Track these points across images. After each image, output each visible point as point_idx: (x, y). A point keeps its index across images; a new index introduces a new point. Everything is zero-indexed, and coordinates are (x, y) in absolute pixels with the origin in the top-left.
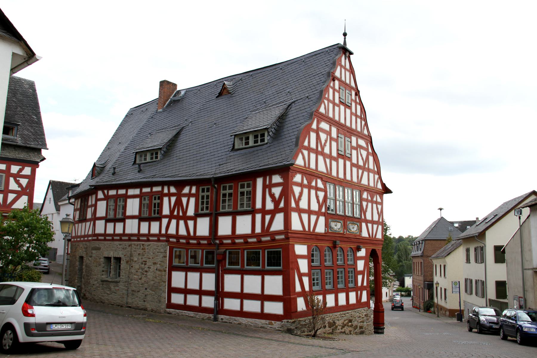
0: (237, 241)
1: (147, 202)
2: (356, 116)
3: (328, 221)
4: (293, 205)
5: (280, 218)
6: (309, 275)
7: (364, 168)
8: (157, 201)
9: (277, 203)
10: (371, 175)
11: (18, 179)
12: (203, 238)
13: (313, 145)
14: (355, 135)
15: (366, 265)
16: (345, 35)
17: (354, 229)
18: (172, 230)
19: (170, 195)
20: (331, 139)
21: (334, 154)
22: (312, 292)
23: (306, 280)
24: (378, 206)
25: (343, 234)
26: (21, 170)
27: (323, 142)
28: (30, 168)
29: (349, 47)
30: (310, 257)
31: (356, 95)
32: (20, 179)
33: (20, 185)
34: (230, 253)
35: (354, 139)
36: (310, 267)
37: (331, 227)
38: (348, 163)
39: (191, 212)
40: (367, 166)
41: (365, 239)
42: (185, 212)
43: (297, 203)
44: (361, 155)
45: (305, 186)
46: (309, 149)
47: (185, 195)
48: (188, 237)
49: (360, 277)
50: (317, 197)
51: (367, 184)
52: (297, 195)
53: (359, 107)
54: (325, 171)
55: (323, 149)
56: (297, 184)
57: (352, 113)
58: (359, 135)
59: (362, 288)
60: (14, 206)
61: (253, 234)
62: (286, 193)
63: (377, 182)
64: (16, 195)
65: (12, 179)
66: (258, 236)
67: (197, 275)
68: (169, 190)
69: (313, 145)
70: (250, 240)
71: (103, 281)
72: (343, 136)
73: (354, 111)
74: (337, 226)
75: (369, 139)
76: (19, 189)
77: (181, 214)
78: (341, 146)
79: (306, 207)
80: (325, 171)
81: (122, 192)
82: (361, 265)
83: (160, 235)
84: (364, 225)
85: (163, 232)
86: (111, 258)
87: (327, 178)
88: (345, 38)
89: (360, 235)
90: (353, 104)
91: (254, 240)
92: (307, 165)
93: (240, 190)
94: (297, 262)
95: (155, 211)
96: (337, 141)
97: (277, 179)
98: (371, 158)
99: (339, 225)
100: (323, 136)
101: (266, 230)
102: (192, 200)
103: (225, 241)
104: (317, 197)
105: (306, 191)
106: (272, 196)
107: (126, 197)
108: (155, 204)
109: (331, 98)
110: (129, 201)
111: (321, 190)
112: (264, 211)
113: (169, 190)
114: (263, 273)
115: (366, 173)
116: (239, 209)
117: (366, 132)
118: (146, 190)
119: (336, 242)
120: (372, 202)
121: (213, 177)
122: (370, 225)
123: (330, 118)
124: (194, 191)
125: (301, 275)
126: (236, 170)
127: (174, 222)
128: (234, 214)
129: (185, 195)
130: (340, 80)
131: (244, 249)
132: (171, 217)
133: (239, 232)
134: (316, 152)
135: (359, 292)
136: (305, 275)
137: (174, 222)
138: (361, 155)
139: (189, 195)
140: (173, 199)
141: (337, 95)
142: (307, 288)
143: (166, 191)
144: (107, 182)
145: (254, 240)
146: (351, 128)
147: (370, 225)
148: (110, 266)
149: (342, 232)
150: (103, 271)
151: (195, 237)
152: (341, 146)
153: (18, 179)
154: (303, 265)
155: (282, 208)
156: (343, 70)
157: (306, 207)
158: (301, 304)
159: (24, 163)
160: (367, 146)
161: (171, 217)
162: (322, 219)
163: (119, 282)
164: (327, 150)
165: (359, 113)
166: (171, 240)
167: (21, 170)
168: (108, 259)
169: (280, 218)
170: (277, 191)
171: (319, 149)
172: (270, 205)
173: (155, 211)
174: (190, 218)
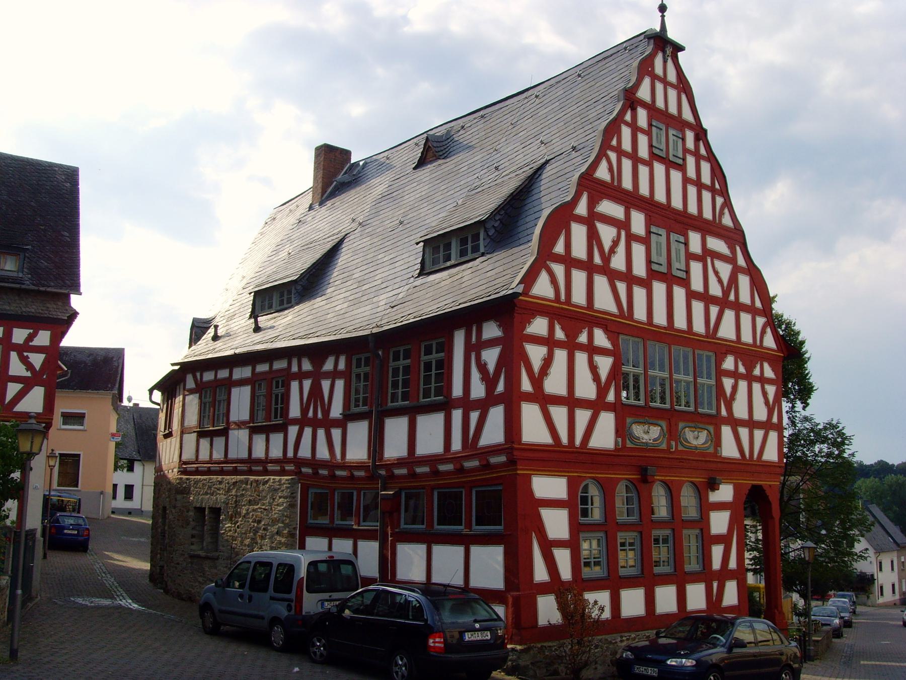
0: (419, 470)
1: (264, 391)
2: (700, 186)
3: (624, 423)
4: (526, 385)
5: (497, 414)
6: (573, 544)
7: (723, 303)
8: (281, 390)
9: (490, 382)
10: (746, 318)
11: (25, 354)
12: (360, 466)
13: (579, 250)
14: (696, 229)
15: (734, 522)
16: (663, 8)
17: (697, 438)
18: (305, 452)
19: (301, 376)
20: (631, 238)
21: (639, 269)
22: (581, 584)
23: (563, 557)
24: (767, 387)
25: (668, 451)
26: (31, 338)
27: (607, 245)
28: (49, 332)
29: (672, 34)
30: (576, 504)
31: (697, 139)
32: (30, 355)
33: (29, 366)
34: (408, 497)
35: (695, 239)
36: (576, 528)
37: (633, 438)
38: (679, 293)
39: (336, 411)
40: (732, 297)
41: (730, 462)
42: (326, 412)
43: (538, 381)
44: (716, 273)
45: (560, 344)
46: (569, 262)
47: (327, 375)
48: (330, 465)
49: (717, 551)
50: (765, 394)
51: (733, 337)
52: (537, 365)
53: (706, 167)
54: (614, 309)
55: (606, 259)
56: (537, 340)
57: (686, 181)
58: (708, 228)
59: (724, 574)
60: (19, 408)
61: (447, 455)
62: (513, 358)
63: (763, 332)
64: (22, 385)
65: (14, 355)
66: (457, 459)
67: (421, 549)
68: (300, 366)
69: (579, 250)
70: (442, 468)
71: (192, 557)
72: (663, 232)
73: (691, 173)
74: (648, 434)
75: (742, 240)
76: (29, 374)
77: (320, 415)
78: (659, 254)
79: (563, 391)
80: (614, 309)
81: (223, 374)
82: (719, 522)
83: (284, 460)
84: (726, 431)
85: (290, 454)
86: (205, 508)
87: (619, 325)
88: (663, 17)
89: (716, 453)
90: (691, 161)
91: (449, 467)
92: (563, 297)
93: (424, 358)
94: (539, 516)
95: (276, 409)
96: (645, 241)
97: (491, 330)
98: (744, 281)
99: (655, 432)
100: (607, 233)
101: (470, 441)
102: (340, 384)
103: (397, 472)
104: (765, 394)
105: (561, 356)
106: (482, 368)
107: (230, 384)
108: (277, 396)
109: (627, 146)
110: (235, 391)
111: (603, 352)
112: (467, 404)
113: (300, 366)
114: (467, 541)
115: (729, 315)
116: (422, 400)
117: (727, 221)
118: (262, 368)
119: (646, 470)
120: (750, 378)
121: (372, 334)
122: (744, 432)
123: (626, 192)
124: (342, 366)
125: (548, 546)
126: (414, 315)
127: (308, 431)
128: (412, 412)
129: (327, 375)
130: (651, 108)
131: (433, 488)
132: (302, 422)
133: (422, 449)
134: (588, 267)
135: (715, 585)
136: (560, 544)
137: (308, 431)
138: (716, 273)
139: (334, 375)
140: (307, 384)
141: (643, 140)
142: (566, 573)
143: (295, 369)
144: (200, 355)
145: (449, 467)
146: (684, 213)
147: (744, 432)
148: (203, 525)
149: (664, 446)
150: (193, 536)
151: (344, 466)
152: (659, 254)
153: (25, 354)
154: (556, 523)
155: (501, 394)
156: (659, 87)
157: (745, 416)
158: (548, 610)
159: (35, 323)
160: (734, 252)
161: (302, 422)
162: (607, 420)
163: (217, 559)
164: (618, 262)
165: (706, 179)
166: (304, 470)
167: (31, 338)
168: (201, 510)
169: (497, 414)
170: (491, 356)
171: (597, 260)
172: (478, 390)
173: (276, 409)
174: (337, 423)
